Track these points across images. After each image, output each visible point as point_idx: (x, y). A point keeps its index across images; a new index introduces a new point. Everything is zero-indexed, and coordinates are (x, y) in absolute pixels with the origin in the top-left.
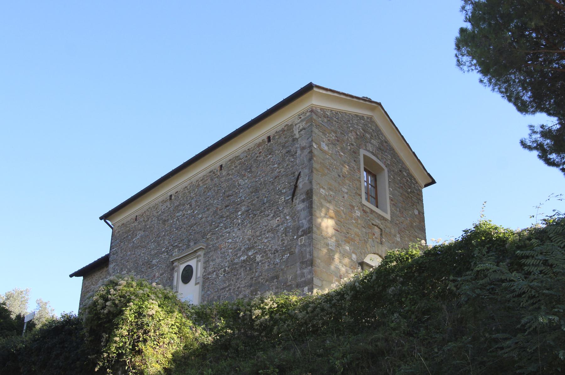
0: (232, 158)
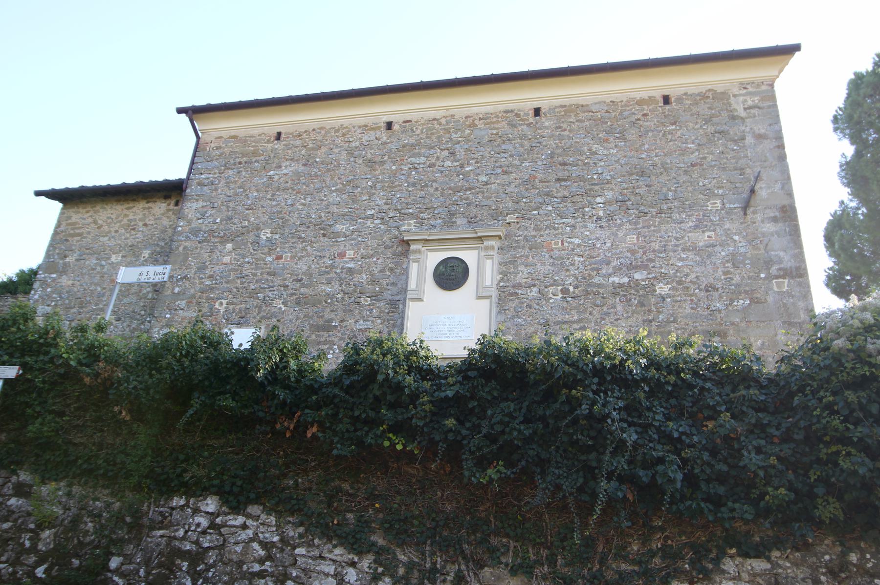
0: (567, 104)
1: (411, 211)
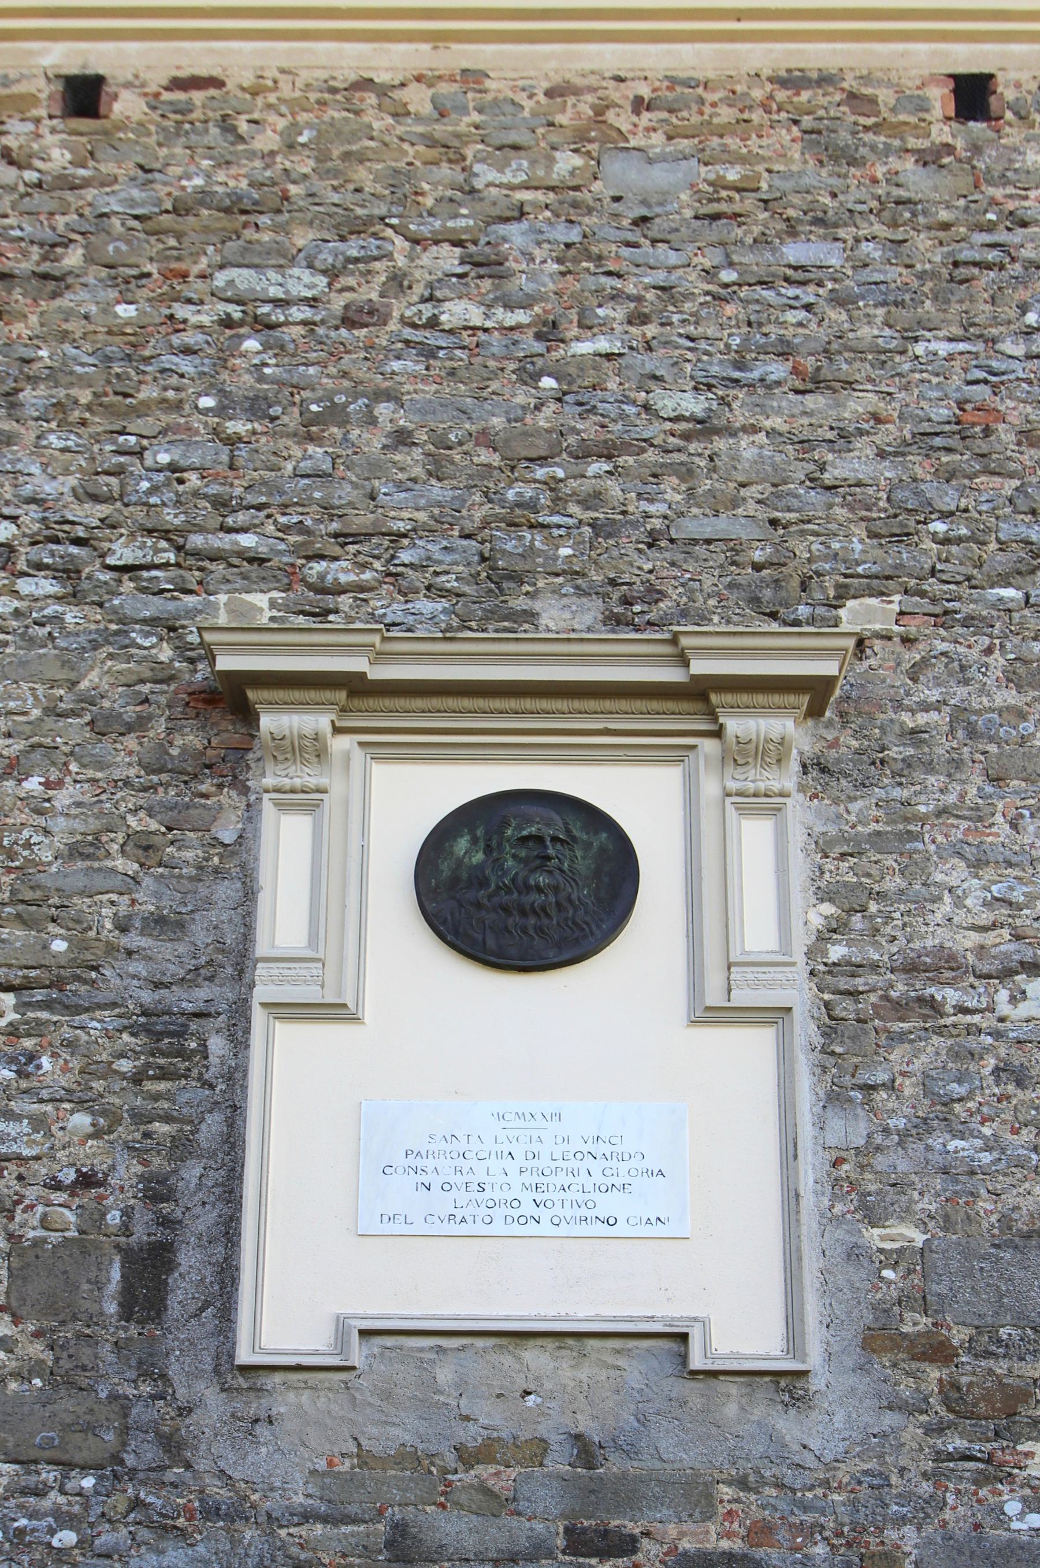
1: (247, 540)
